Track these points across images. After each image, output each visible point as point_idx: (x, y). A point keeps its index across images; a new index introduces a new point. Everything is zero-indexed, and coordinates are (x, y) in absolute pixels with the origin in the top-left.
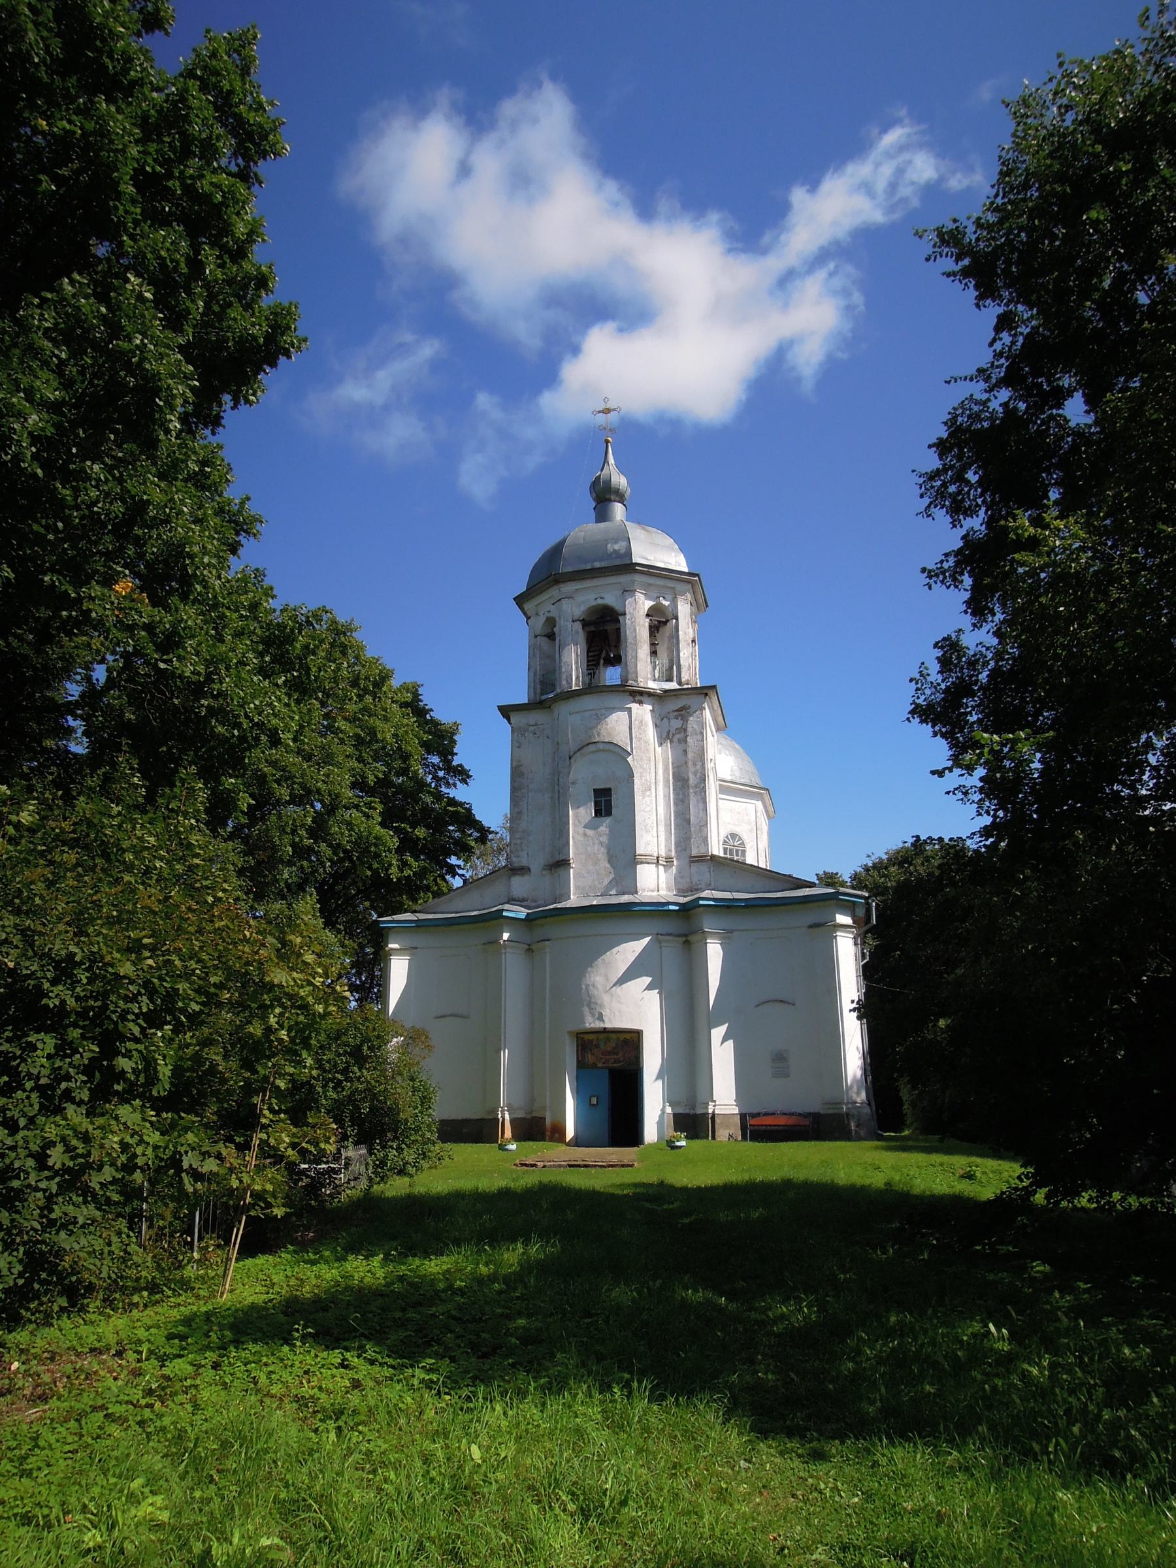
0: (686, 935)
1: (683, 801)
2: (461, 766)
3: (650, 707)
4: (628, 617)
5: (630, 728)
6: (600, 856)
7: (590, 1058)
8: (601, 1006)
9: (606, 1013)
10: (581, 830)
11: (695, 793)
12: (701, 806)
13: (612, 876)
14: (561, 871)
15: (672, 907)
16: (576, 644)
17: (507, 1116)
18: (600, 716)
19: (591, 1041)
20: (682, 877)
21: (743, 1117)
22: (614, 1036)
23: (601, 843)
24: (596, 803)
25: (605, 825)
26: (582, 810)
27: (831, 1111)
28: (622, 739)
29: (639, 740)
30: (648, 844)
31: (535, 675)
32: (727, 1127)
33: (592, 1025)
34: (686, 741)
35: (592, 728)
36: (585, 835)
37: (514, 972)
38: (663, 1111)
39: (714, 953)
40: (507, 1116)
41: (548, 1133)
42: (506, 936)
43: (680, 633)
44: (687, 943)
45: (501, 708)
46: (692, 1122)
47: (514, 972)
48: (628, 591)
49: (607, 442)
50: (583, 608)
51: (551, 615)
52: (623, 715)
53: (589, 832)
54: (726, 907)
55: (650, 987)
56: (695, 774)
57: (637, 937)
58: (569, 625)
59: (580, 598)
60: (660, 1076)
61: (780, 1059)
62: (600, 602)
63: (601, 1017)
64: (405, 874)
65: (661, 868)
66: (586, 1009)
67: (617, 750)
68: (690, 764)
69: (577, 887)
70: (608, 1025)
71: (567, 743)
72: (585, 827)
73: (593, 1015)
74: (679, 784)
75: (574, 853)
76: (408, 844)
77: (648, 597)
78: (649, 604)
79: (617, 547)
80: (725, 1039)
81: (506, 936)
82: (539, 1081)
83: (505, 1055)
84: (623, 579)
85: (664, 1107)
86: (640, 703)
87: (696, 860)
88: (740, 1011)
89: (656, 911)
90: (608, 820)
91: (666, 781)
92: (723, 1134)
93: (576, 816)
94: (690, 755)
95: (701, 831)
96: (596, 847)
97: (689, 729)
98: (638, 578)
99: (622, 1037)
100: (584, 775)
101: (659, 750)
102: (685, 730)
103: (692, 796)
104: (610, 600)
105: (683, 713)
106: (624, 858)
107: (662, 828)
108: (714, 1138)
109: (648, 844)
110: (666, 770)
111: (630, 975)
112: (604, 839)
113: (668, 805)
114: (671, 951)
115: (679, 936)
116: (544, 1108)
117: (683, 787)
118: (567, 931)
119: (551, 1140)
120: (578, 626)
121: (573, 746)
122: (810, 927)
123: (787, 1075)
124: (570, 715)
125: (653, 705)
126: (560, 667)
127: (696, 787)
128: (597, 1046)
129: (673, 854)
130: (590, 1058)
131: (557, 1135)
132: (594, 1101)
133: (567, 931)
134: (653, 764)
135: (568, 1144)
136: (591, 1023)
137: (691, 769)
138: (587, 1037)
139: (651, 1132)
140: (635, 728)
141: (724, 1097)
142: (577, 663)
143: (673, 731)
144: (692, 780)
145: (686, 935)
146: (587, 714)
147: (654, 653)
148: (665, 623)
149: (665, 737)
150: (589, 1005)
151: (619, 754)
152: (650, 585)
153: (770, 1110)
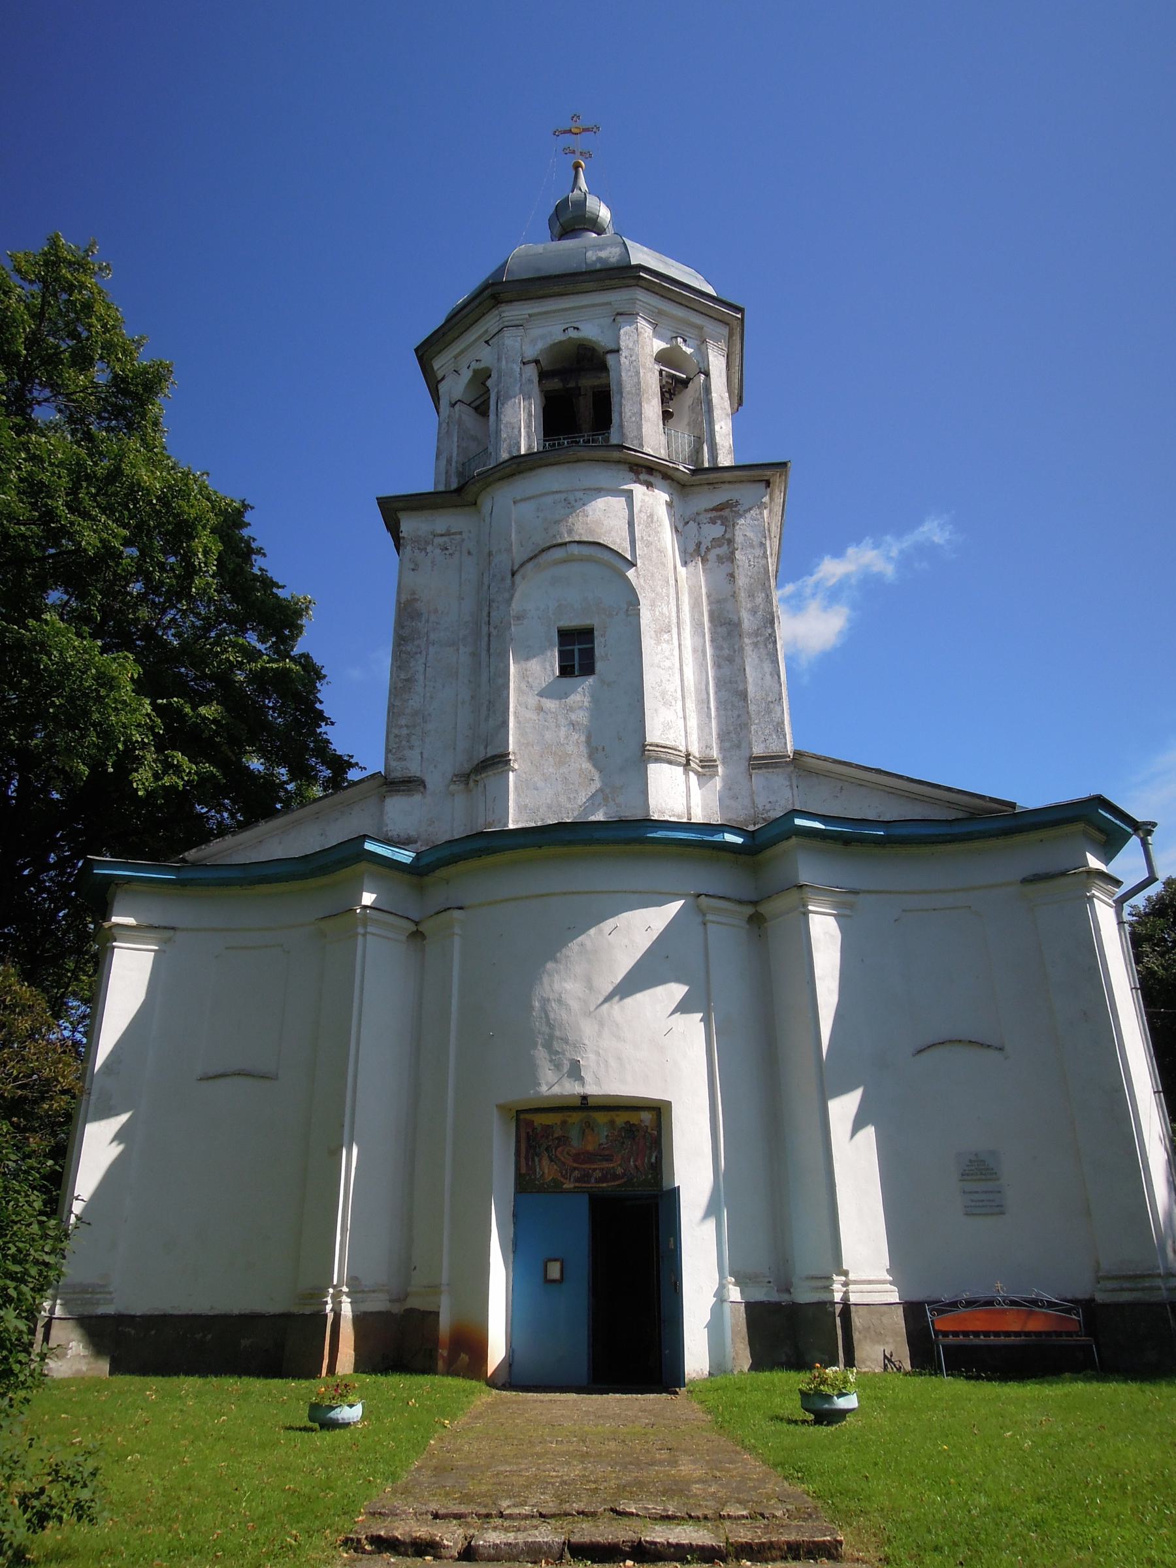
0: (754, 903)
1: (730, 660)
2: (306, 656)
3: (665, 497)
4: (624, 353)
5: (631, 524)
6: (570, 749)
7: (546, 1169)
8: (578, 1046)
9: (588, 1062)
10: (533, 700)
11: (756, 645)
12: (767, 667)
13: (597, 785)
14: (489, 778)
15: (730, 838)
16: (527, 397)
17: (347, 1309)
18: (574, 502)
19: (548, 1128)
20: (735, 798)
21: (913, 1311)
22: (601, 1118)
23: (573, 724)
24: (561, 653)
25: (582, 692)
26: (534, 665)
27: (1125, 1297)
28: (617, 539)
29: (648, 544)
30: (668, 726)
31: (449, 461)
32: (879, 1337)
33: (556, 1090)
34: (731, 558)
35: (557, 522)
36: (540, 709)
37: (380, 973)
38: (720, 1296)
39: (824, 932)
40: (347, 1309)
41: (444, 1352)
42: (368, 898)
43: (714, 395)
44: (757, 921)
45: (383, 503)
46: (792, 1329)
47: (380, 973)
48: (626, 315)
49: (577, 166)
50: (540, 345)
51: (482, 365)
52: (619, 503)
53: (550, 704)
54: (847, 839)
55: (683, 1007)
56: (754, 611)
57: (658, 898)
58: (517, 368)
59: (535, 332)
60: (712, 1210)
61: (979, 1171)
62: (573, 334)
63: (575, 1071)
64: (167, 781)
65: (693, 777)
66: (541, 1054)
67: (606, 556)
68: (743, 595)
69: (517, 803)
70: (594, 1087)
71: (509, 550)
72: (541, 694)
73: (558, 1067)
74: (723, 630)
75: (518, 743)
76: (178, 734)
77: (657, 334)
78: (659, 345)
79: (603, 254)
80: (858, 1126)
81: (368, 898)
82: (421, 1217)
83: (351, 1159)
84: (617, 298)
85: (722, 1286)
86: (649, 485)
87: (761, 763)
88: (898, 1063)
89: (691, 845)
90: (590, 680)
91: (698, 626)
92: (870, 1354)
93: (523, 676)
94: (742, 581)
95: (769, 711)
96: (563, 732)
97: (739, 539)
98: (641, 295)
99: (621, 1119)
100: (540, 603)
101: (682, 571)
102: (730, 542)
103: (748, 650)
104: (591, 331)
105: (726, 513)
106: (625, 749)
107: (691, 705)
108: (850, 1362)
109: (668, 726)
110: (696, 605)
111: (640, 978)
112: (581, 717)
113: (702, 666)
114: (726, 935)
115: (740, 902)
116: (434, 1289)
117: (729, 634)
118: (514, 875)
119: (451, 1372)
120: (531, 372)
121: (519, 555)
122: (1025, 881)
123: (999, 1210)
124: (513, 509)
125: (670, 495)
126: (498, 432)
127: (756, 633)
128: (563, 1140)
129: (715, 753)
130: (546, 1169)
131: (464, 1357)
132: (554, 1271)
133: (514, 875)
134: (672, 591)
135: (492, 1383)
136: (553, 1085)
137: (745, 604)
138: (540, 1120)
139: (696, 1358)
140: (638, 521)
141: (865, 1264)
142: (528, 426)
143: (706, 543)
144: (748, 622)
145: (754, 903)
146: (549, 500)
147: (667, 415)
148: (685, 383)
149: (691, 552)
150: (548, 1046)
151: (612, 564)
152: (660, 313)
153: (982, 1294)
